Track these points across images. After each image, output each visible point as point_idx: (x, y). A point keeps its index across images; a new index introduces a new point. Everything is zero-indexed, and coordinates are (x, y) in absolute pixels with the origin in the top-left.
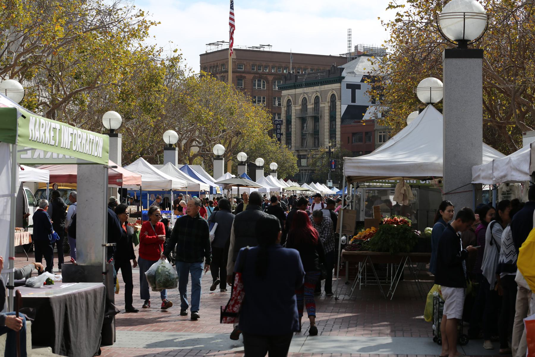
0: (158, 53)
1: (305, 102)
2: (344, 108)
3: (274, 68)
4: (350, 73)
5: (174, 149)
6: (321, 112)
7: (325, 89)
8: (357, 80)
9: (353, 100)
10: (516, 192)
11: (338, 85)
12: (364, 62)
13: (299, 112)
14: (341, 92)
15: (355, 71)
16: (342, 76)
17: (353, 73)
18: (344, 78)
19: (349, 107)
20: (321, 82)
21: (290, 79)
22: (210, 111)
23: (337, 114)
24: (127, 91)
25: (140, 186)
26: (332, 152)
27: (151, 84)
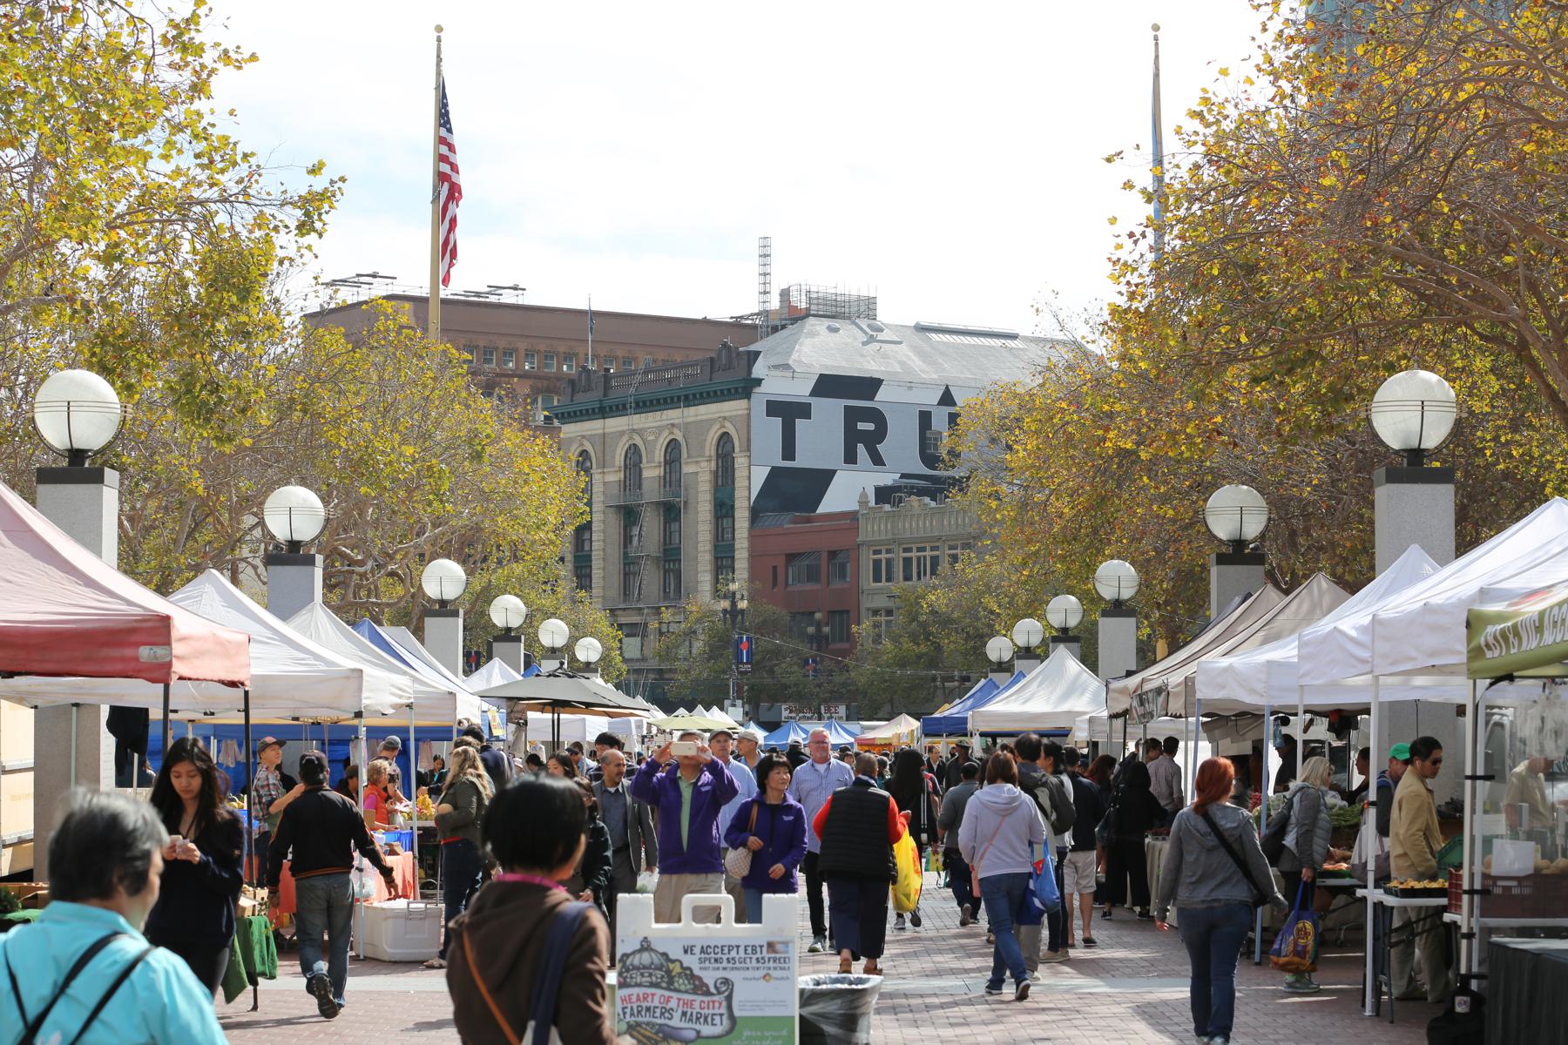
0: (241, 186)
1: (634, 459)
2: (760, 476)
3: (533, 356)
4: (776, 367)
5: (310, 561)
6: (686, 490)
7: (699, 418)
8: (800, 390)
9: (789, 451)
11: (743, 403)
12: (818, 334)
13: (616, 491)
14: (749, 426)
15: (790, 362)
16: (754, 375)
17: (787, 367)
18: (758, 382)
19: (775, 473)
20: (686, 397)
21: (588, 389)
22: (404, 442)
23: (738, 494)
24: (120, 331)
25: (239, 692)
26: (742, 611)
27: (223, 298)
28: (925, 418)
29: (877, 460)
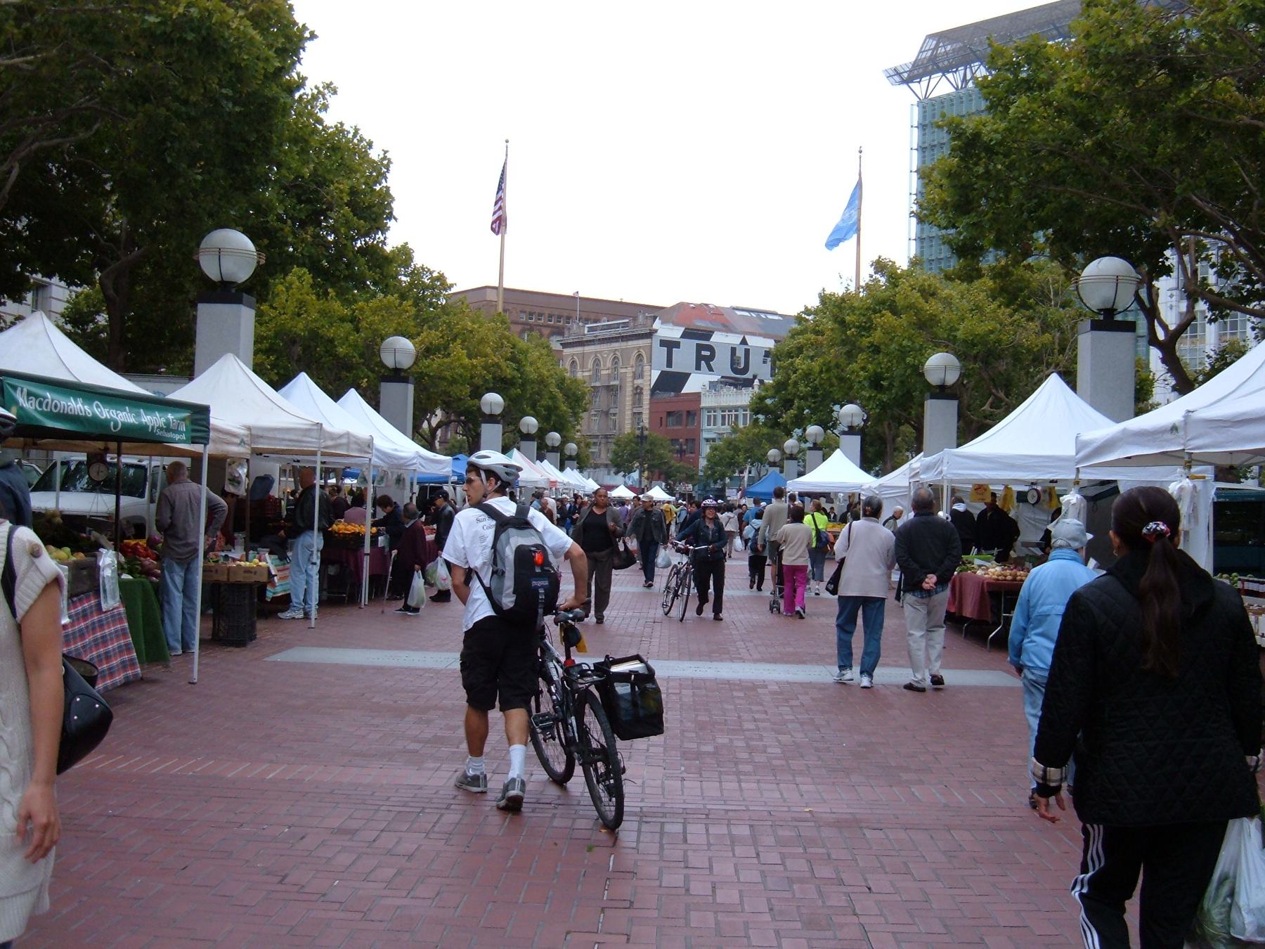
2: (655, 375)
9: (669, 364)
10: (234, 449)
11: (648, 341)
18: (656, 331)
19: (663, 372)
28: (733, 350)
29: (711, 369)
